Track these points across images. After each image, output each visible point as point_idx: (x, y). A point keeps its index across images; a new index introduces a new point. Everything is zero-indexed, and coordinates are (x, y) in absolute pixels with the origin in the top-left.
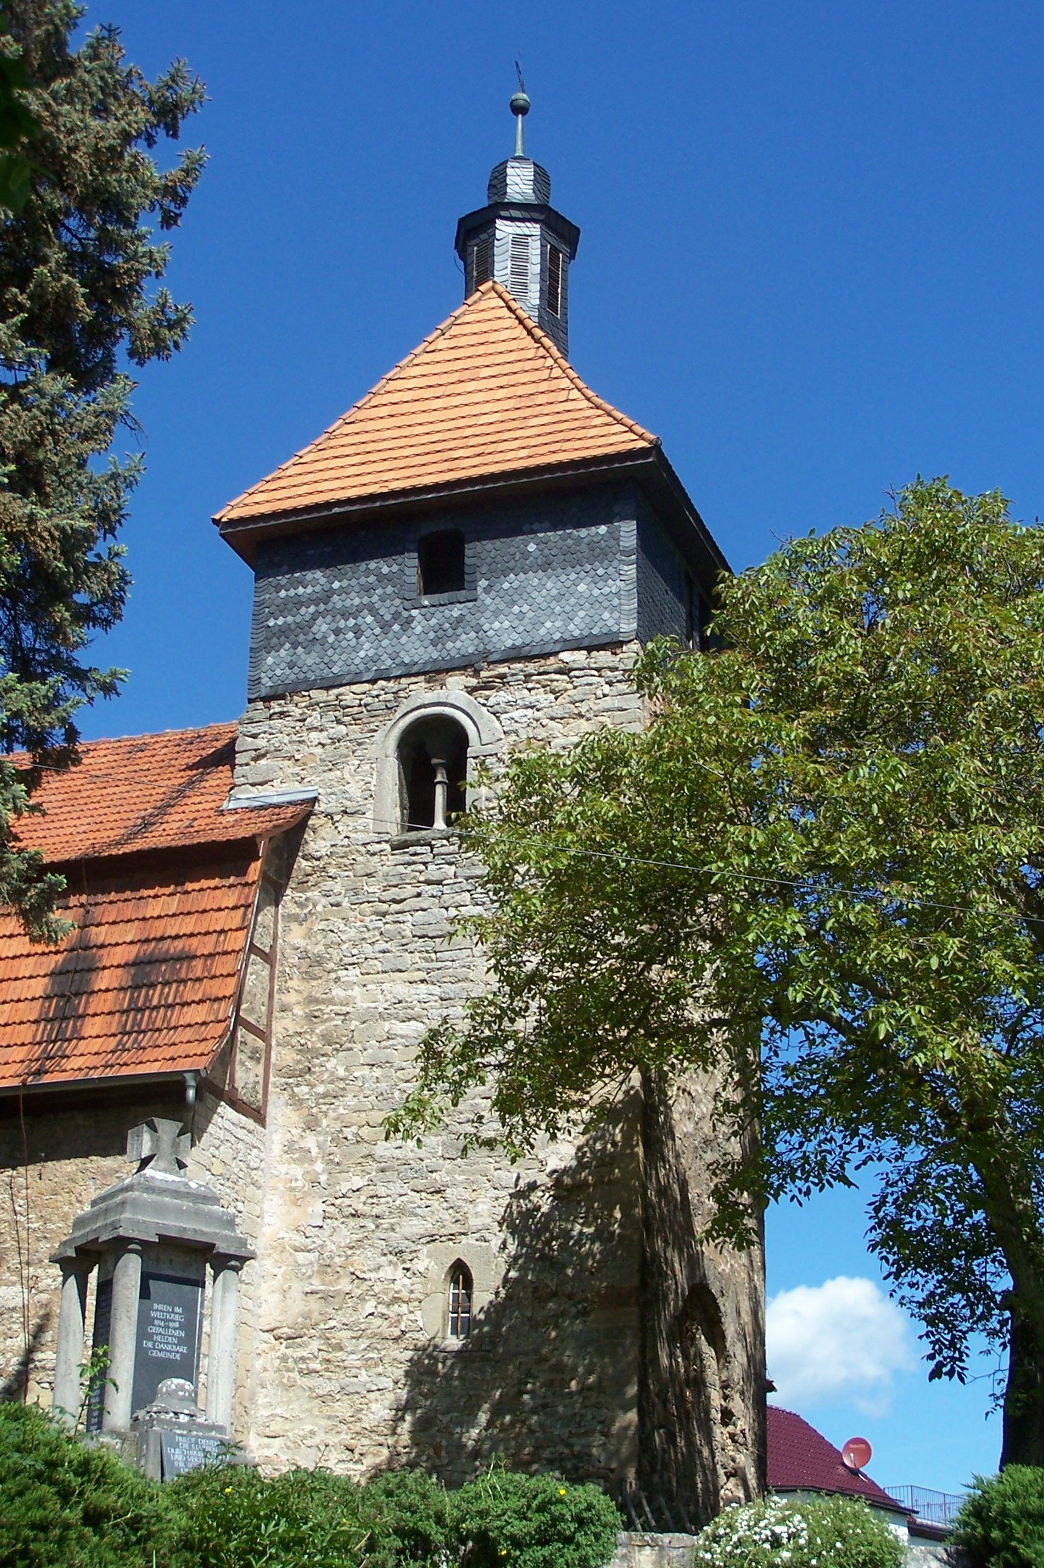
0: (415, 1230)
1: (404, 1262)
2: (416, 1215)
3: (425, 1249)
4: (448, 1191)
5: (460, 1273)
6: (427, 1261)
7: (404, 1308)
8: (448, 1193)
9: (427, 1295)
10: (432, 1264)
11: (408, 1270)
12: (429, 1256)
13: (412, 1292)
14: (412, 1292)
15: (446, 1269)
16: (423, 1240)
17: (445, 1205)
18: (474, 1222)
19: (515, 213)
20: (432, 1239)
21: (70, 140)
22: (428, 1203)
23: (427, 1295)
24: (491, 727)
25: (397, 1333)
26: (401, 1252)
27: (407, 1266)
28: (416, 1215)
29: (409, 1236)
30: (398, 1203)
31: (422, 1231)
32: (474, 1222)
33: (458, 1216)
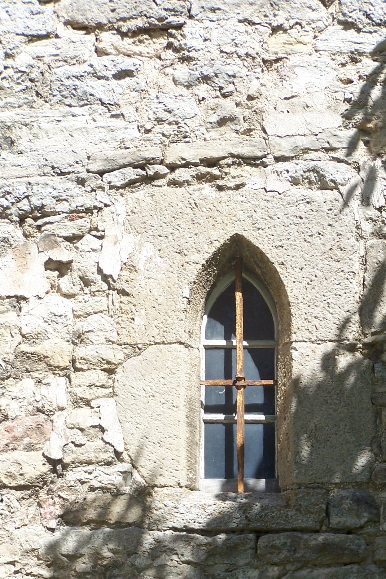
0: (83, 145)
1: (51, 241)
2: (86, 100)
3: (122, 204)
4: (191, 27)
5: (242, 288)
6: (128, 243)
7: (56, 391)
8: (192, 35)
9: (136, 349)
10: (157, 251)
11: (61, 267)
12: (131, 228)
13: (79, 338)
14: (79, 338)
15: (193, 272)
16: (116, 178)
17: (182, 71)
18: (284, 127)
19: (241, 462)
20: (145, 174)
21: (296, 330)
22: (126, 63)
23: (136, 349)
24: (246, 15)
25: (34, 466)
26: (40, 212)
27: (62, 254)
28: (86, 100)
29: (63, 161)
30: (23, 60)
31: (110, 151)
32: (284, 127)
33: (228, 107)
